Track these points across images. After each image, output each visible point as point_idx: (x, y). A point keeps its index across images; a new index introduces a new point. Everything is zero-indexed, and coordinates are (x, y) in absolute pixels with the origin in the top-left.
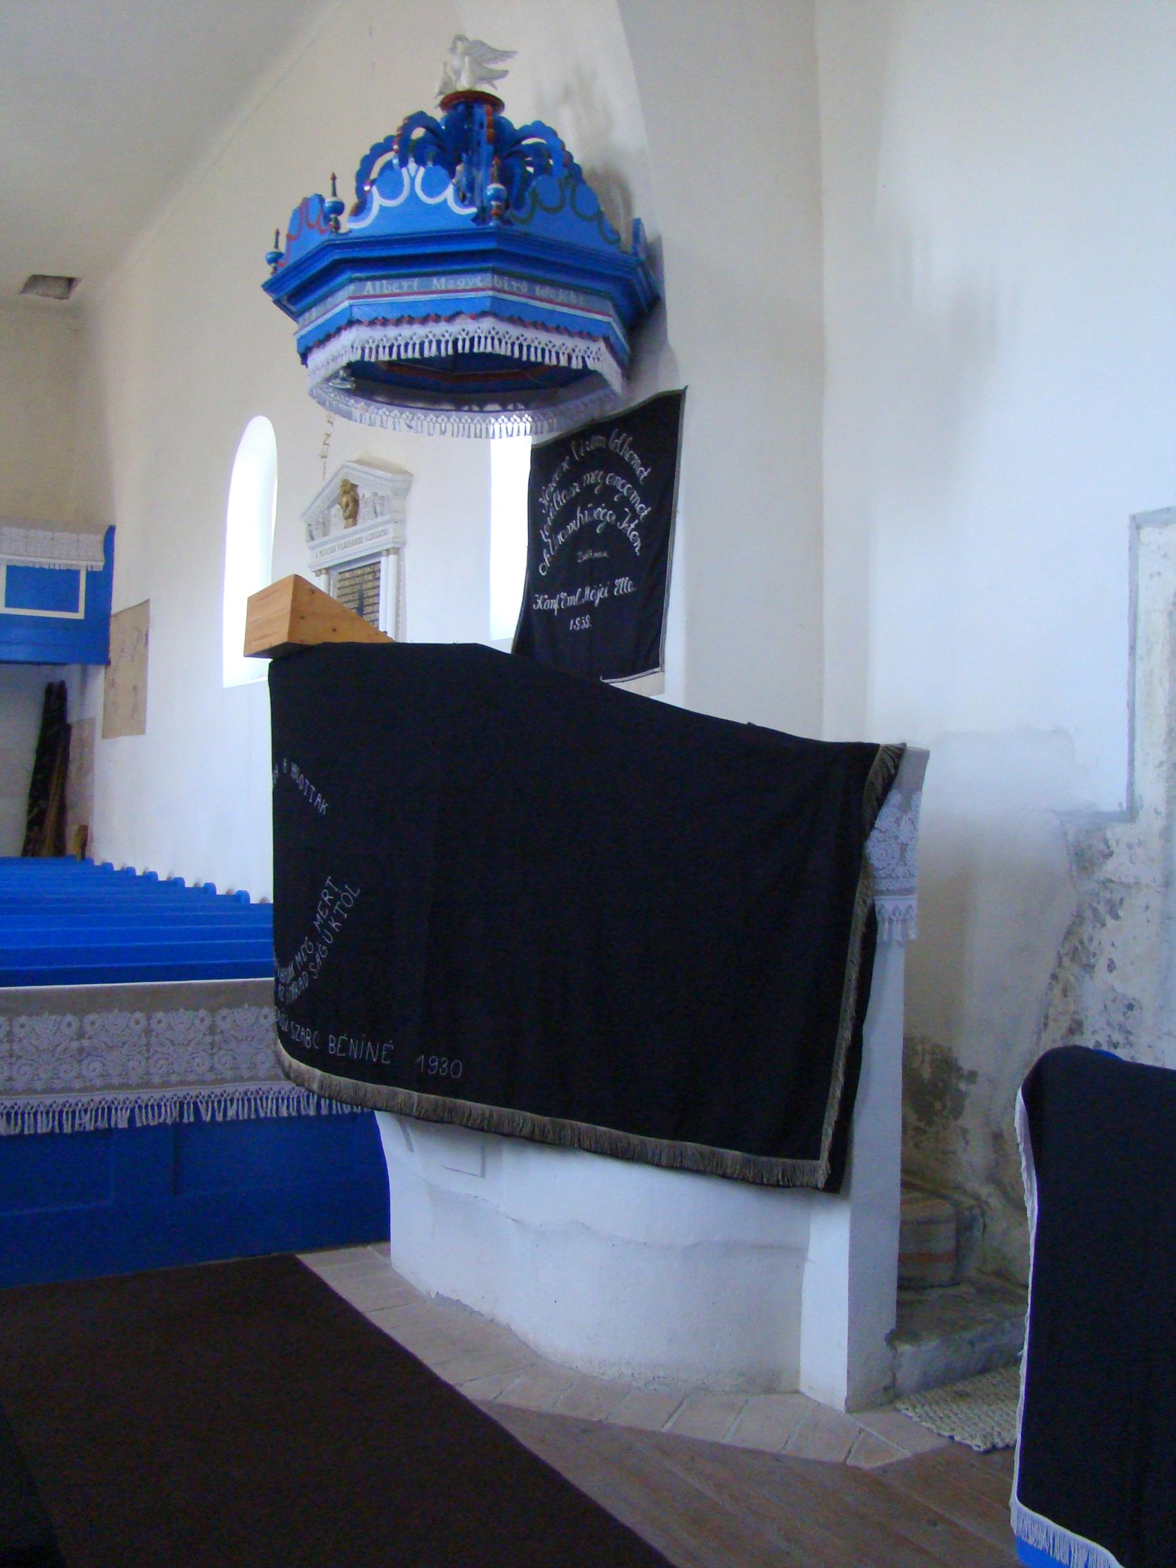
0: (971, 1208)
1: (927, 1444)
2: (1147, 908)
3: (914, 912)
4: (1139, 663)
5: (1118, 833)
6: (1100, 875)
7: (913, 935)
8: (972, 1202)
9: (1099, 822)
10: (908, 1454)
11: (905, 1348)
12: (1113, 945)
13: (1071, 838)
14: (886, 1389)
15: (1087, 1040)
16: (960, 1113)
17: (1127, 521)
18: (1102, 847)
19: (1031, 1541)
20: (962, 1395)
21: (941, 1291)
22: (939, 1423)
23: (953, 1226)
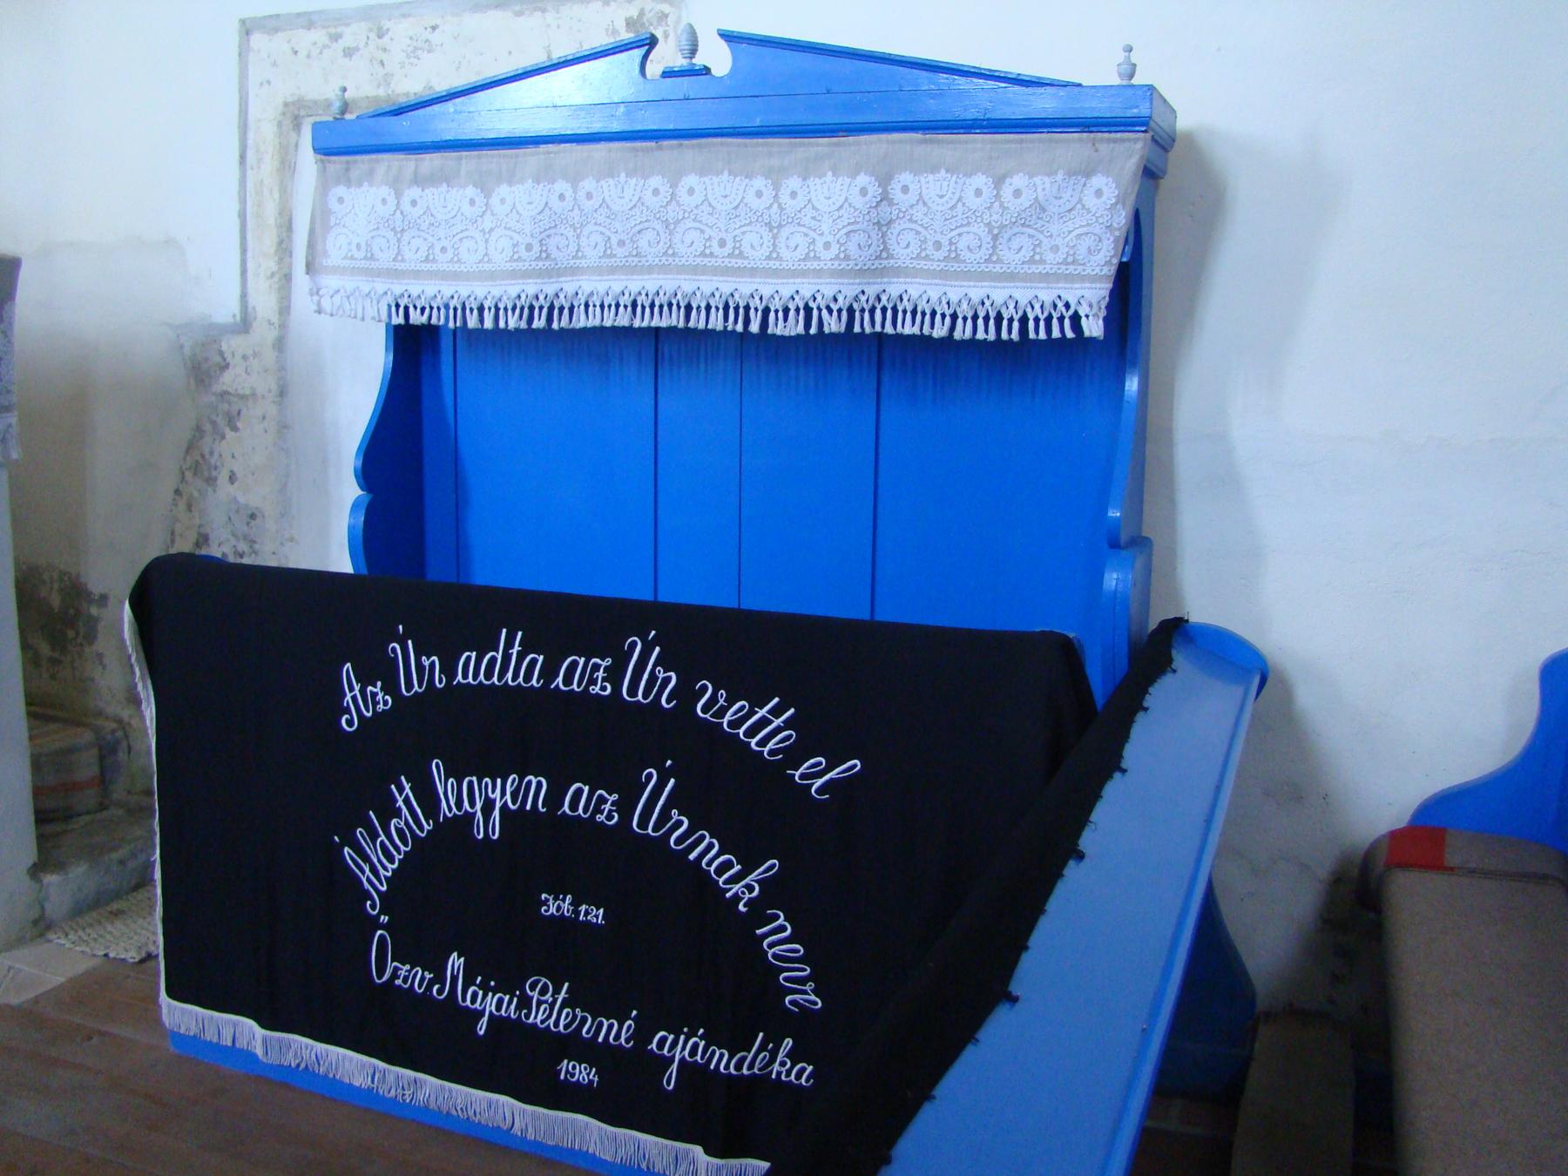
0: (113, 732)
1: (83, 966)
3: (15, 430)
4: (249, 172)
5: (234, 345)
6: (217, 388)
7: (15, 455)
8: (114, 725)
9: (212, 336)
10: (62, 980)
11: (51, 879)
13: (187, 351)
14: (35, 922)
15: (216, 552)
16: (95, 637)
17: (236, 25)
18: (218, 359)
19: (182, 1031)
20: (117, 914)
21: (87, 818)
22: (92, 944)
23: (95, 751)
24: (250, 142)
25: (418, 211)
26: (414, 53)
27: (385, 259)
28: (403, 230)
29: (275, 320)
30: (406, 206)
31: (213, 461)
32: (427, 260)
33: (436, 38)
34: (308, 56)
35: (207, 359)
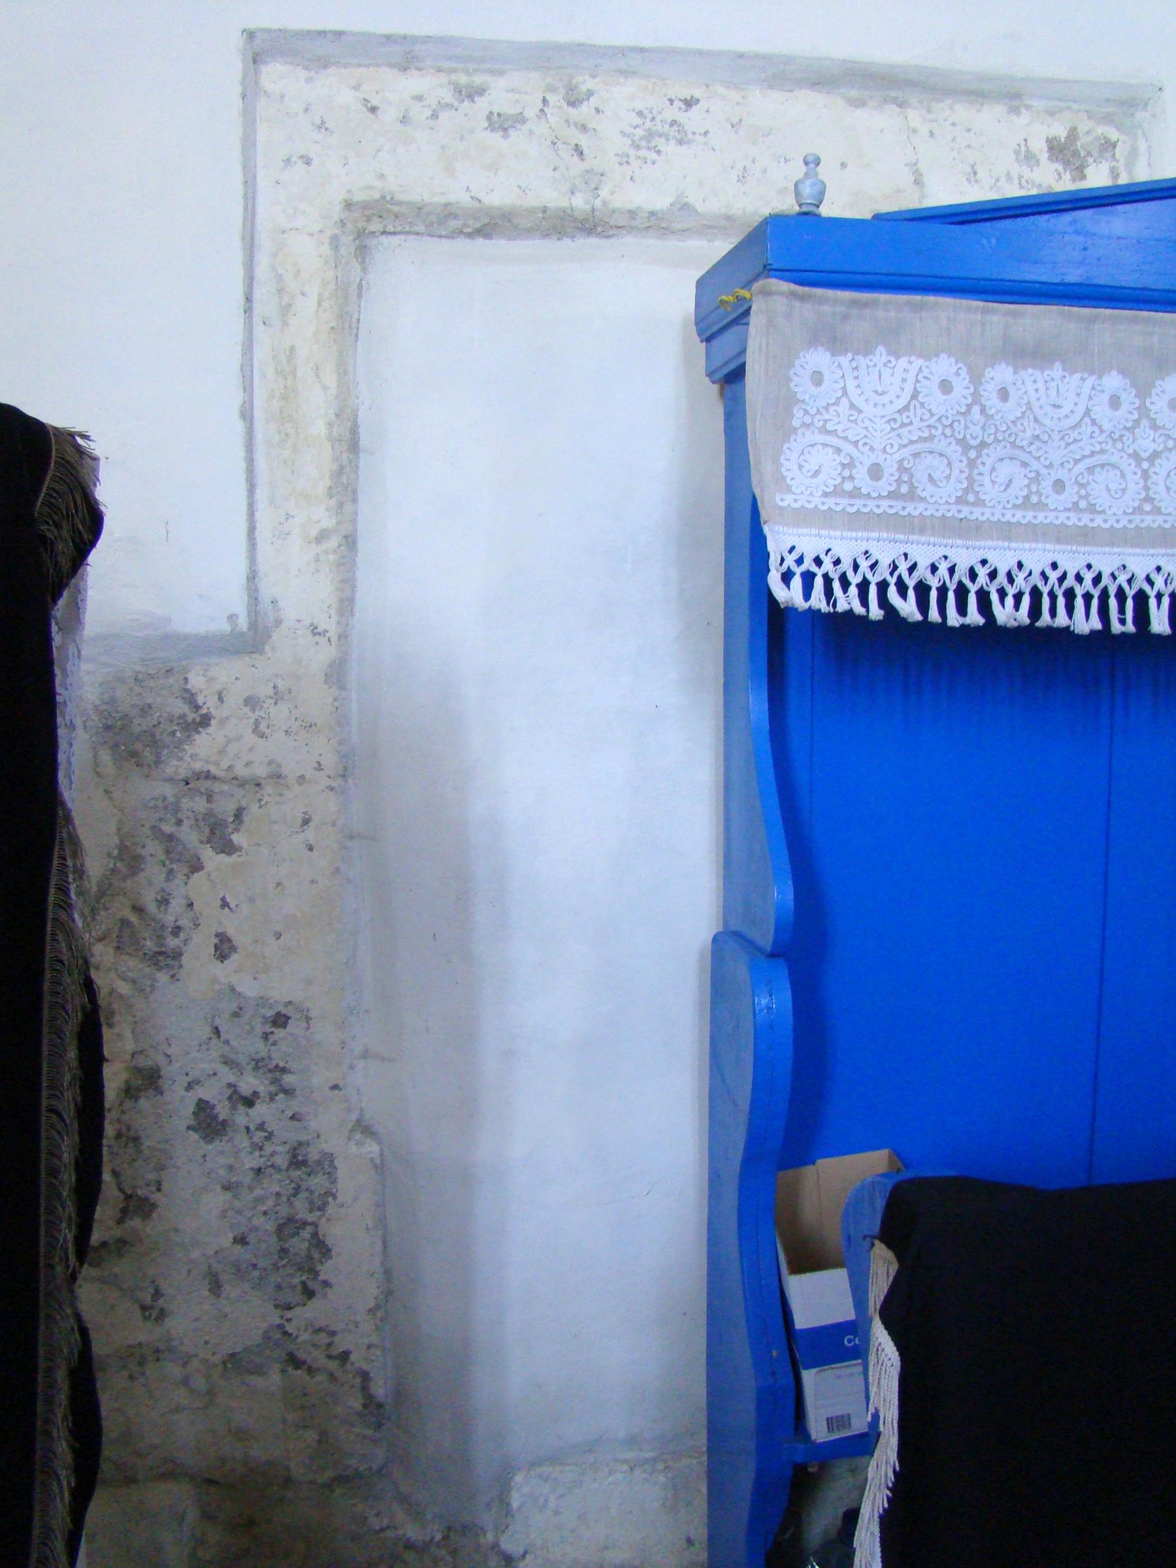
2: (306, 822)
4: (259, 331)
6: (178, 767)
12: (225, 904)
17: (236, 40)
18: (180, 707)
24: (262, 271)
25: (1012, 410)
26: (648, 139)
27: (940, 497)
28: (983, 445)
29: (329, 624)
30: (992, 401)
31: (169, 919)
32: (1026, 504)
33: (693, 120)
34: (404, 120)
35: (146, 710)
